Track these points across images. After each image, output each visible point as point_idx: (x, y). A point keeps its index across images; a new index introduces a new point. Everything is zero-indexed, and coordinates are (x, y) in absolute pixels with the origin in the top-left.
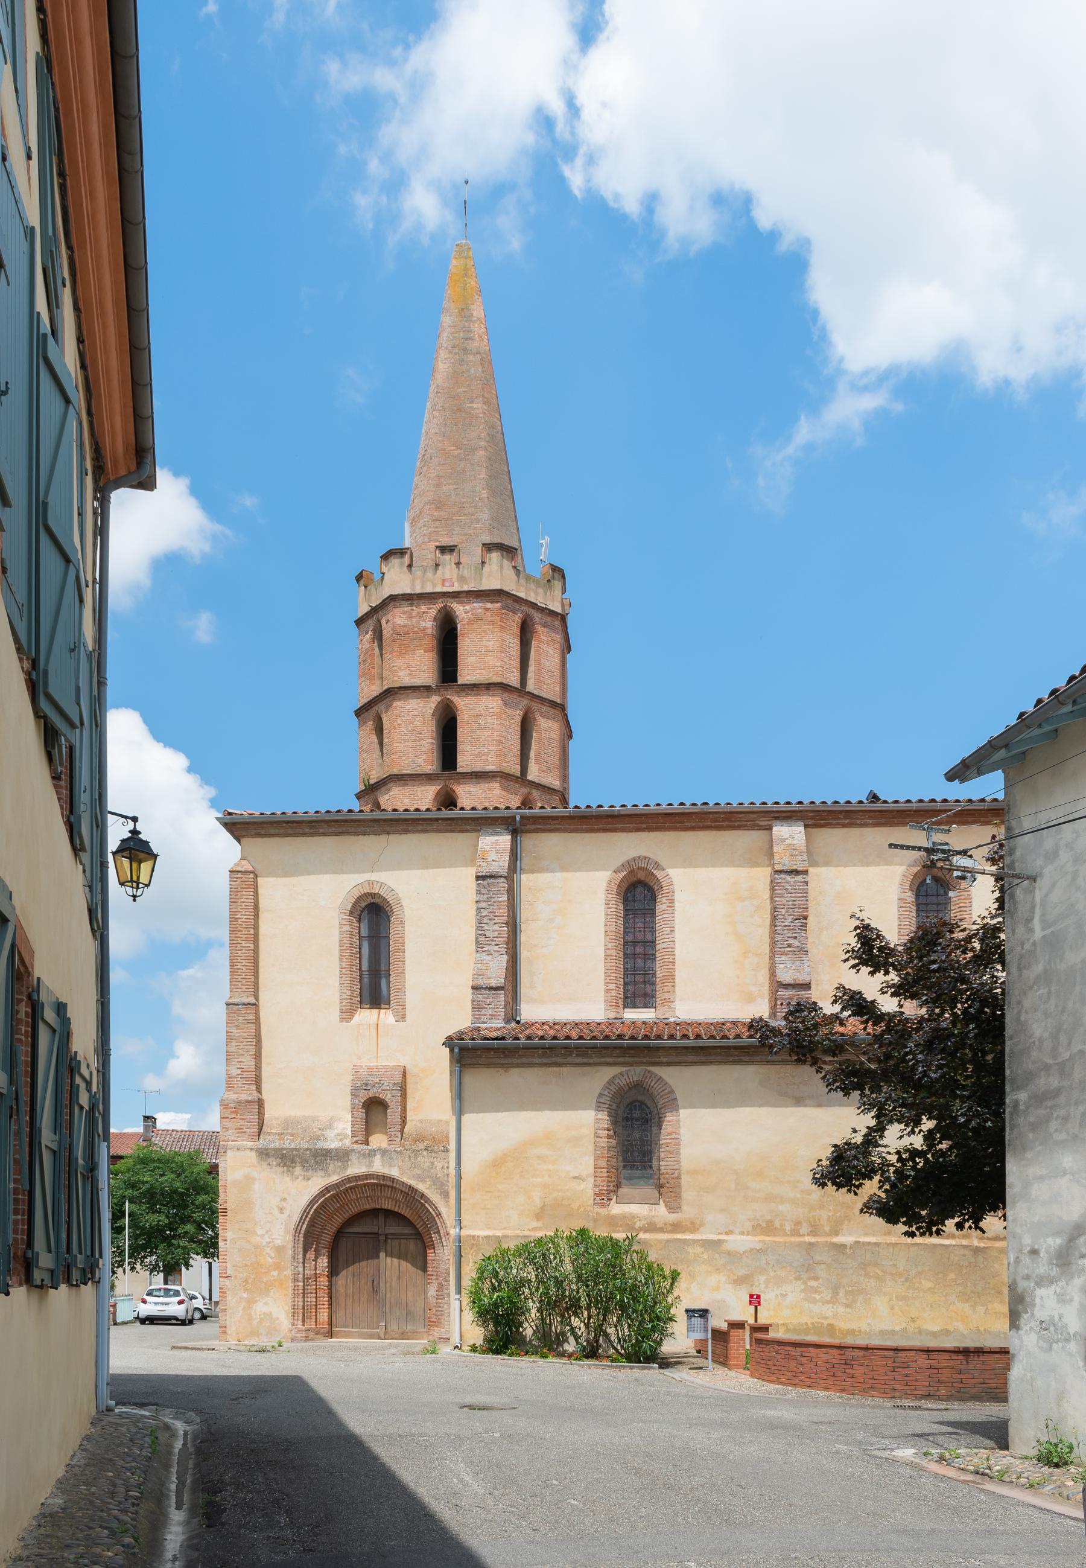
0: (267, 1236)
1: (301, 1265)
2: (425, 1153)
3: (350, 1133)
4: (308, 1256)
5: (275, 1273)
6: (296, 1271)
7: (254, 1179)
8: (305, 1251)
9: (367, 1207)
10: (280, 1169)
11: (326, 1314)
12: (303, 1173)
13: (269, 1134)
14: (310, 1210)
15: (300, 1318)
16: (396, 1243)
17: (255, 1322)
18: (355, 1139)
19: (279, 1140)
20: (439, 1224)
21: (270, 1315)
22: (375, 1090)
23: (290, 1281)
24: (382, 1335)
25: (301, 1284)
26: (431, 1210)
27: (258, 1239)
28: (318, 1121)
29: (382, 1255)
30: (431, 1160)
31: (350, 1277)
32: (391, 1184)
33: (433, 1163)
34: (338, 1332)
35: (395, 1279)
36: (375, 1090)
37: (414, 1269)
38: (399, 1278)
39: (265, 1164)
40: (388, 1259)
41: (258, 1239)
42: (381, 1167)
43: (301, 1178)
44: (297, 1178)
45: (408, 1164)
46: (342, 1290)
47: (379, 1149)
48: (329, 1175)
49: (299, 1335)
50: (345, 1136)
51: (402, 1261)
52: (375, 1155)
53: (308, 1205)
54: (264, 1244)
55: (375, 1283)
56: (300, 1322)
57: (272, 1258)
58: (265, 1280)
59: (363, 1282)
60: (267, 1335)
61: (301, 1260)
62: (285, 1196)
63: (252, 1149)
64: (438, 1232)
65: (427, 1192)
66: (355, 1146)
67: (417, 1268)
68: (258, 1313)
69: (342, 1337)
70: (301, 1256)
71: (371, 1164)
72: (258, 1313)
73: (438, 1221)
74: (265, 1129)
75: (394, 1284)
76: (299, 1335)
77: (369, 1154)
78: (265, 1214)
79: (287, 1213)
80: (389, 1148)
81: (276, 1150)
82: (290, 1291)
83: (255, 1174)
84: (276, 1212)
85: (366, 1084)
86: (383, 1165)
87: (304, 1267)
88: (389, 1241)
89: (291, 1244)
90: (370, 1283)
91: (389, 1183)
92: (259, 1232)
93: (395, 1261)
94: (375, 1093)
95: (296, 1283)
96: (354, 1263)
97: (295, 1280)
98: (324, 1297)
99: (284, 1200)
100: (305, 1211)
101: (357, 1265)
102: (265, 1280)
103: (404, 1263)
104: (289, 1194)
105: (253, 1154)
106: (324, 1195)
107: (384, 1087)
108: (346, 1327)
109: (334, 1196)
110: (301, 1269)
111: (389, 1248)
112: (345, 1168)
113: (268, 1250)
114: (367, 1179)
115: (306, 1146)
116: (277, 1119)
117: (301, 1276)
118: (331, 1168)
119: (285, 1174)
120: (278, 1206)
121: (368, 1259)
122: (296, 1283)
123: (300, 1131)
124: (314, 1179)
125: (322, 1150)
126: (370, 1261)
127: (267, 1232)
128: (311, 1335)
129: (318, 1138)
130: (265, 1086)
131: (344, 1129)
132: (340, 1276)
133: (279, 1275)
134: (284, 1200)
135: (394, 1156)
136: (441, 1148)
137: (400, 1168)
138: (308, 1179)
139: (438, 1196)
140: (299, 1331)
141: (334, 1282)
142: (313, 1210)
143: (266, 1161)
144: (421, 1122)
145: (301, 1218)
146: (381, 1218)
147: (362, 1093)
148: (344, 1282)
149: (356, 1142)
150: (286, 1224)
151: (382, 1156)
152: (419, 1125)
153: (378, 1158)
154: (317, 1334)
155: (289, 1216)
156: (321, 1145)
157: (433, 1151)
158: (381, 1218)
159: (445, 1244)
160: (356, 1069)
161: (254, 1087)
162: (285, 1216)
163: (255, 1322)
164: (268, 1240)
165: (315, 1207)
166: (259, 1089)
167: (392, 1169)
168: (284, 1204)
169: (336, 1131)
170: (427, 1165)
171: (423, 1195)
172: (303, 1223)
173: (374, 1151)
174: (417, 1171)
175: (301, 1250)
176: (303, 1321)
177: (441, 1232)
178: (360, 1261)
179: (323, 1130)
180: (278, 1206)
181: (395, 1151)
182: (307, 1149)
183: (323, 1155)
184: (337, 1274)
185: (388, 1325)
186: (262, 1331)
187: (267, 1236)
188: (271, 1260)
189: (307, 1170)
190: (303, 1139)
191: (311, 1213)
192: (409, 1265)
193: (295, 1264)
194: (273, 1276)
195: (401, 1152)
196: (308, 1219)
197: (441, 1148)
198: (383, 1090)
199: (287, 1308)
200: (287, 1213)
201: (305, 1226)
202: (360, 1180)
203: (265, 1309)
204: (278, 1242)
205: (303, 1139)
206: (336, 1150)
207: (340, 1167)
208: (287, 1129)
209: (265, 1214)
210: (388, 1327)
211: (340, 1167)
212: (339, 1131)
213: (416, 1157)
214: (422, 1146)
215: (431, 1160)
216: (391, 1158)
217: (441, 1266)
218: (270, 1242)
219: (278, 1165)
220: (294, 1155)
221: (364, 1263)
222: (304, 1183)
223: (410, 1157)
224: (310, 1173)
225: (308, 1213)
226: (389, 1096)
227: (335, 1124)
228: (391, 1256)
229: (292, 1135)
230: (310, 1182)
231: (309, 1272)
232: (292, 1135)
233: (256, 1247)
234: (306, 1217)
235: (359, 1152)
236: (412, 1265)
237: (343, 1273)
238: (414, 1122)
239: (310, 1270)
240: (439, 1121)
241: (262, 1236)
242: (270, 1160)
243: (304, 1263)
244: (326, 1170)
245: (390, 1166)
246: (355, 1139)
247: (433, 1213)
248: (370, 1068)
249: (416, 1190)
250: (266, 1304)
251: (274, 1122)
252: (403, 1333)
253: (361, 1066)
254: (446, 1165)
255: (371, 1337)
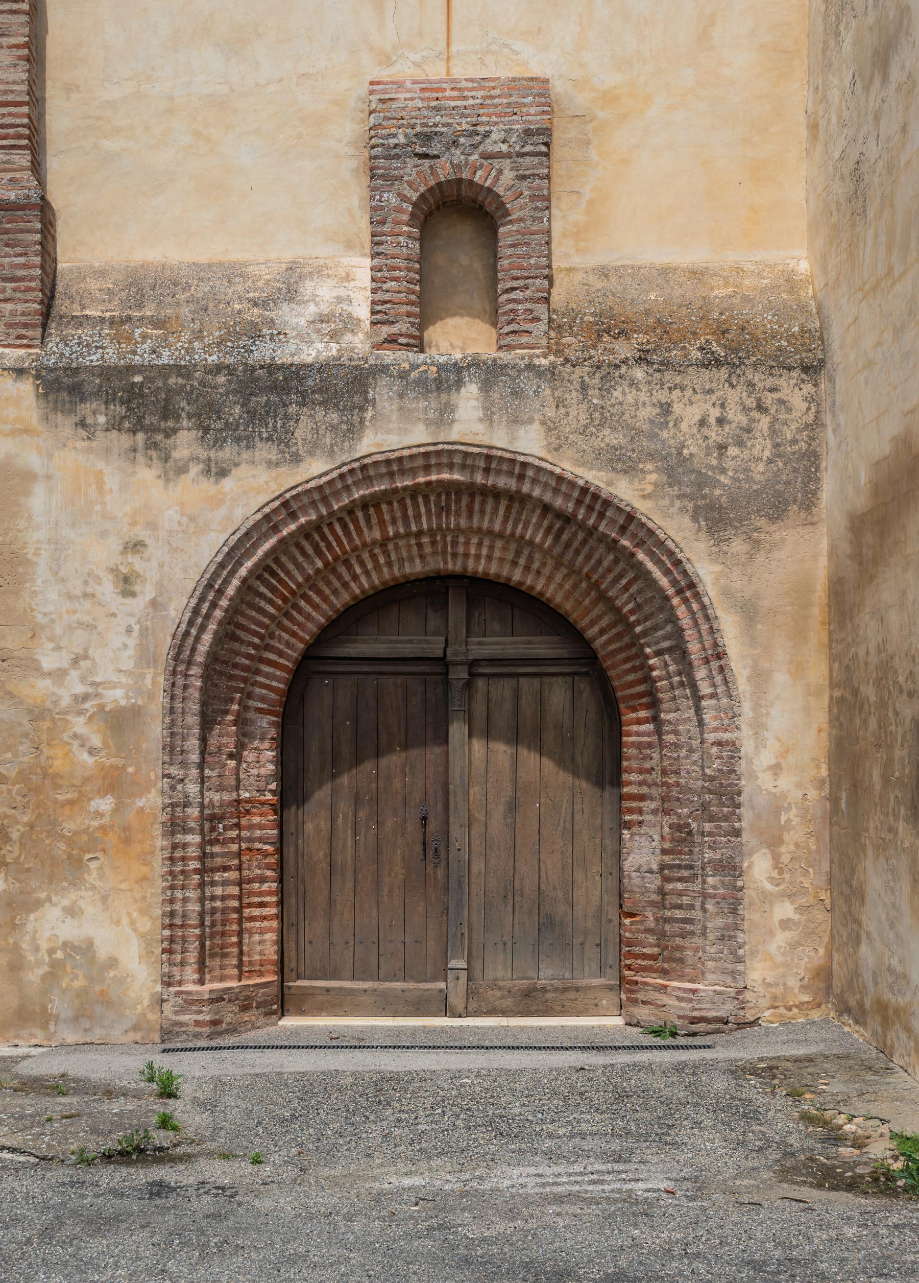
0: (74, 674)
1: (194, 772)
2: (639, 373)
3: (363, 312)
4: (213, 742)
5: (105, 804)
6: (178, 797)
7: (28, 477)
8: (207, 723)
9: (416, 568)
10: (125, 441)
11: (271, 937)
12: (203, 454)
13: (80, 322)
14: (226, 582)
15: (192, 957)
16: (503, 690)
17: (34, 977)
18: (386, 330)
19: (117, 339)
20: (685, 622)
21: (86, 949)
22: (458, 156)
23: (157, 830)
24: (457, 1000)
25: (194, 839)
26: (657, 573)
27: (44, 685)
28: (244, 276)
29: (457, 730)
30: (662, 396)
31: (345, 807)
32: (512, 484)
33: (666, 408)
34: (305, 994)
35: (499, 810)
36: (458, 156)
37: (565, 777)
38: (513, 807)
39: (66, 424)
40: (478, 746)
41: (44, 685)
42: (480, 428)
43: (195, 469)
44: (182, 470)
45: (578, 413)
46: (319, 853)
47: (475, 363)
48: (296, 459)
49: (186, 1018)
50: (349, 324)
51: (523, 752)
52: (459, 383)
53: (222, 565)
54: (65, 702)
55: (433, 825)
56: (190, 973)
57: (92, 751)
58: (68, 827)
59: (389, 823)
60: (76, 1018)
61: (195, 757)
62: (143, 534)
63: (20, 372)
64: (680, 651)
65: (642, 507)
66: (388, 356)
67: (575, 773)
68: (44, 946)
69: (319, 1010)
70: (193, 743)
71: (445, 415)
72: (44, 946)
73: (681, 611)
74: (62, 306)
75: (497, 826)
76: (186, 1018)
77: (438, 382)
78: (70, 597)
79: (147, 592)
80: (506, 357)
81: (106, 372)
82: (159, 866)
83: (33, 460)
84: (107, 589)
85: (426, 138)
86: (488, 418)
87: (202, 780)
88: (481, 683)
89: (161, 700)
90: (412, 827)
91: (503, 482)
92: (48, 661)
93: (501, 751)
94: (458, 167)
95: (179, 838)
96: (358, 761)
97: (174, 826)
98: (263, 880)
99: (136, 546)
100: (209, 586)
101: (368, 766)
102: (68, 827)
103: (530, 759)
104: (153, 526)
105: (26, 388)
106: (275, 529)
107: (489, 147)
108: (334, 975)
109: (305, 532)
110: (193, 789)
111: (479, 708)
112: (353, 431)
113: (79, 724)
114: (427, 468)
115: (213, 359)
116: (102, 274)
117: (194, 812)
118: (302, 431)
119: (141, 459)
120: (114, 571)
121: (406, 747)
122: (179, 838)
123: (185, 311)
124: (243, 471)
125: (272, 368)
126: (414, 753)
127: (75, 661)
128: (229, 1014)
129: (254, 332)
130: (54, 164)
131: (339, 300)
132: (310, 806)
133: (116, 810)
134: (136, 546)
135: (528, 383)
136: (696, 355)
137: (550, 427)
138: (223, 473)
139: (687, 521)
140: (190, 1002)
141: (291, 828)
142: (235, 582)
143: (72, 411)
144: (603, 272)
145: (196, 611)
146: (456, 611)
147: (410, 168)
148: (324, 825)
149: (391, 341)
150: (144, 632)
151: (486, 386)
152: (599, 284)
153: (471, 389)
154: (245, 1008)
155: (154, 603)
156: (263, 352)
157: (666, 364)
158: (456, 611)
159: (705, 689)
160: (15, 381)
161: (23, 159)
162: (138, 604)
163: (34, 977)
164: (79, 689)
165: (243, 572)
166: (37, 167)
167: (521, 431)
168: (136, 562)
169: (312, 308)
170: (648, 412)
171: (630, 517)
172: (202, 629)
173: (457, 368)
174: (611, 437)
175: (193, 720)
176: (202, 967)
177: (693, 647)
178: (378, 754)
179: (265, 305)
180: (114, 571)
181: (530, 367)
182: (218, 369)
183: (274, 387)
184: (302, 799)
185: (478, 965)
186: (58, 1005)
187: (74, 674)
188: (90, 760)
189: (218, 443)
190: (199, 335)
191: (231, 591)
192: (548, 764)
193: (174, 771)
194: (99, 814)
195: (552, 370)
196: (218, 614)
197: (696, 355)
198: (486, 156)
199: (145, 925)
200: (147, 592)
201: (207, 638)
202: (403, 472)
203: (68, 931)
204: (116, 697)
205: (199, 335)
206: (323, 368)
207: (333, 428)
208: (140, 306)
209: (70, 597)
210: (477, 974)
211: (333, 428)
212: (325, 309)
213: (605, 391)
214: (624, 349)
215: (662, 396)
216: (516, 394)
217: (686, 765)
218: (86, 697)
219: (115, 425)
220: (169, 391)
221: (393, 761)
222: (208, 486)
223: (584, 387)
224: (228, 452)
225: (220, 592)
226: (508, 176)
227: (308, 287)
228: (488, 735)
229: (158, 323)
230: (228, 484)
231: (217, 797)
232: (158, 323)
233: (38, 714)
234: (214, 605)
235: (403, 375)
236: (560, 763)
237: (322, 794)
238: (579, 277)
239: (221, 788)
240: (665, 271)
241: (59, 675)
242: (86, 409)
243: (201, 766)
244: (283, 439)
245: (515, 421)
246: (386, 330)
247: (664, 582)
248: (428, 88)
249: (607, 503)
250: (72, 911)
251: (93, 285)
252: (528, 993)
253: (400, 84)
254: (715, 413)
255: (419, 1007)
